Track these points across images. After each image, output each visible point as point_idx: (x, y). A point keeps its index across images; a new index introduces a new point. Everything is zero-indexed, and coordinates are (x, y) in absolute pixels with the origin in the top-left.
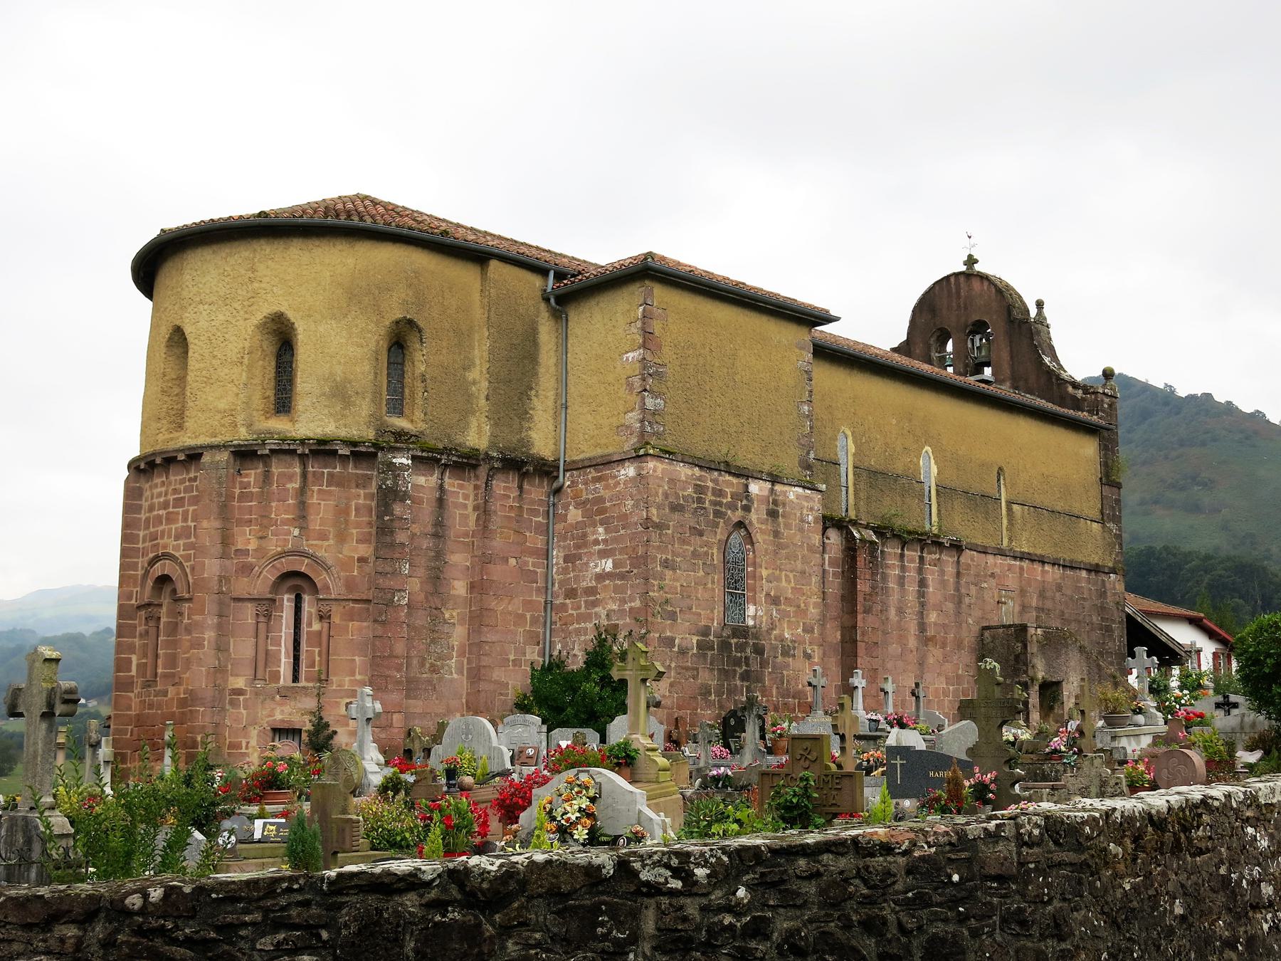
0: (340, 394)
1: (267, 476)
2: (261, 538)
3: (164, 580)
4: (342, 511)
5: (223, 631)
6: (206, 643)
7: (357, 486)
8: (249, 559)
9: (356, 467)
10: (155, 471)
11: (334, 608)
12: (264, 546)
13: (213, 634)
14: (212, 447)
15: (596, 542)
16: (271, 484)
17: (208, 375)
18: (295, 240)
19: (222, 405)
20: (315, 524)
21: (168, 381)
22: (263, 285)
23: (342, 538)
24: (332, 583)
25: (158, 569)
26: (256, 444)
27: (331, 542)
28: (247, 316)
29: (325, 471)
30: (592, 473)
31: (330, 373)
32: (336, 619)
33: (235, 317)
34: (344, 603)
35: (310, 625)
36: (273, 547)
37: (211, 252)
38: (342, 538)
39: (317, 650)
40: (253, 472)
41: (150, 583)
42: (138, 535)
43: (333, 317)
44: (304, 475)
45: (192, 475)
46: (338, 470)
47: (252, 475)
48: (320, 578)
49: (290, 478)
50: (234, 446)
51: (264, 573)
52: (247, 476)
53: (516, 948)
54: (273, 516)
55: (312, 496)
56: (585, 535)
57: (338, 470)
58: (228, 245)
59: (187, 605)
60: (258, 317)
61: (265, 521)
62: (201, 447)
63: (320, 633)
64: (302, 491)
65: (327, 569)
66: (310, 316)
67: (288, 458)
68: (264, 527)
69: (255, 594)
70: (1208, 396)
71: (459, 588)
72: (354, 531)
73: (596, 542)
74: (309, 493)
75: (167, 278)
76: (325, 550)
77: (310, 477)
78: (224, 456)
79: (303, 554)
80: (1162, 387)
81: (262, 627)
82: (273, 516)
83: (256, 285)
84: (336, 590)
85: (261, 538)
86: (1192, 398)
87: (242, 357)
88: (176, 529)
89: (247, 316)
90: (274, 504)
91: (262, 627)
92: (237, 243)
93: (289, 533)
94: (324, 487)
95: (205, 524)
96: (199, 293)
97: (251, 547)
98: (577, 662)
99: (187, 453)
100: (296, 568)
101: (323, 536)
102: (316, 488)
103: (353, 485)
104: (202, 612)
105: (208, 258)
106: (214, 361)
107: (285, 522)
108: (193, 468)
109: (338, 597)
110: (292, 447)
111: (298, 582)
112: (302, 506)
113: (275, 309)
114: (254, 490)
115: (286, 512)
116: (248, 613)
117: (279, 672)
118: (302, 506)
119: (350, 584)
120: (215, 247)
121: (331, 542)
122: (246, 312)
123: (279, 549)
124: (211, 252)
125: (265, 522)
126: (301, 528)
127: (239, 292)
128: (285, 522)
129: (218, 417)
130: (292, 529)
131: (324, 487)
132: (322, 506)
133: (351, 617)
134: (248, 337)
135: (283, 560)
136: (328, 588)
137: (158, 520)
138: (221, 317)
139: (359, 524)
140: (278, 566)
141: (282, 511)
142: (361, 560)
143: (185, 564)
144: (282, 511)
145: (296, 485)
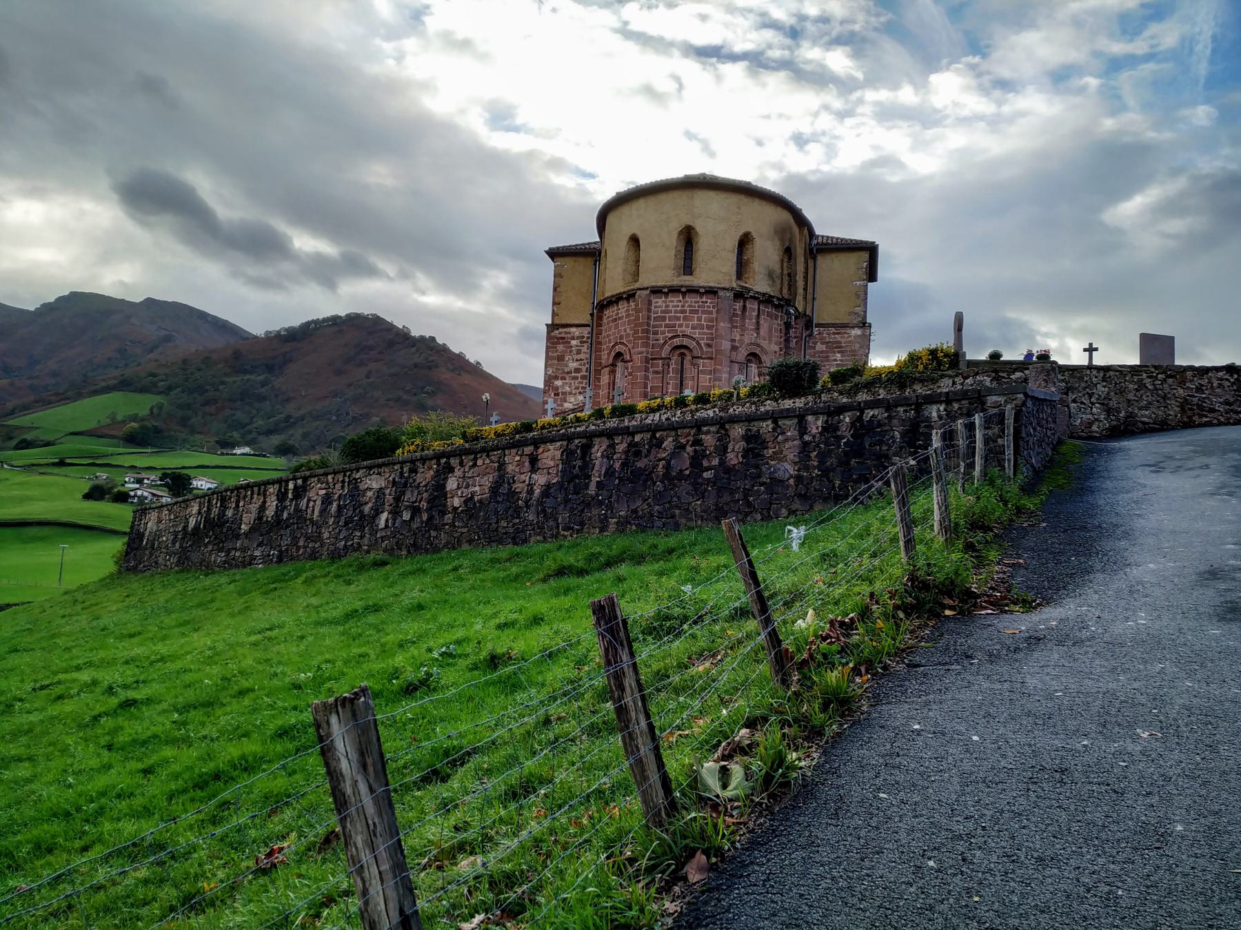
3: (619, 355)
14: (724, 289)
15: (836, 360)
20: (762, 332)
23: (770, 341)
25: (618, 349)
30: (833, 330)
41: (613, 354)
45: (704, 300)
48: (764, 358)
49: (754, 310)
53: (834, 679)
56: (828, 357)
65: (766, 353)
68: (743, 330)
70: (433, 339)
71: (514, 570)
73: (836, 360)
76: (764, 344)
78: (730, 294)
79: (758, 345)
80: (472, 361)
86: (422, 338)
95: (722, 324)
139: (777, 336)
141: (750, 324)
144: (750, 324)
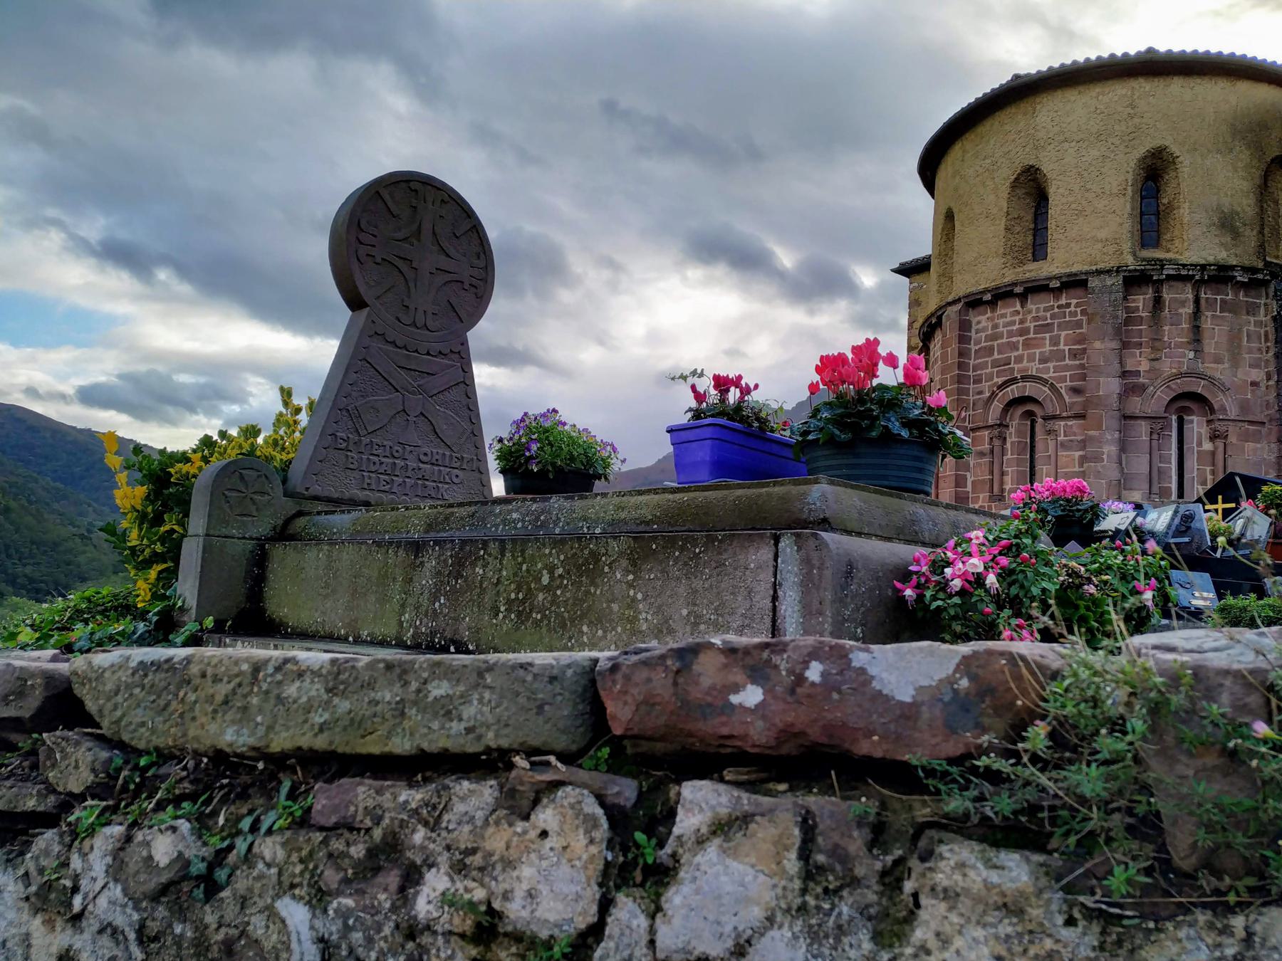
0: (1227, 224)
1: (1158, 302)
2: (1153, 360)
4: (1234, 339)
5: (1123, 447)
6: (1105, 457)
7: (1248, 313)
8: (1141, 380)
9: (1246, 296)
10: (999, 303)
11: (1230, 429)
12: (1157, 367)
13: (1113, 448)
14: (1099, 272)
16: (1162, 310)
17: (1079, 208)
18: (1176, 79)
19: (1102, 234)
20: (1209, 346)
21: (1011, 220)
22: (1144, 120)
24: (1228, 404)
26: (1153, 270)
27: (1226, 365)
28: (1128, 150)
29: (1218, 297)
31: (1218, 205)
32: (1233, 439)
33: (1113, 151)
34: (1241, 424)
35: (1200, 444)
36: (1167, 367)
37: (1077, 93)
38: (1235, 362)
39: (1208, 469)
40: (1141, 297)
42: (970, 349)
43: (1219, 151)
44: (1197, 301)
46: (1230, 297)
47: (1141, 301)
48: (1217, 399)
49: (1183, 303)
50: (1130, 271)
51: (1158, 393)
52: (1134, 301)
54: (1166, 339)
55: (1206, 321)
57: (1230, 297)
58: (1100, 85)
59: (1062, 423)
60: (1141, 151)
61: (1157, 344)
62: (1087, 273)
63: (1213, 453)
64: (1197, 314)
66: (1196, 150)
67: (1180, 285)
69: (1150, 411)
72: (1247, 356)
74: (1203, 318)
75: (944, 176)
76: (1220, 371)
77: (1203, 302)
79: (1201, 376)
81: (1155, 443)
82: (1166, 339)
83: (1136, 120)
84: (1233, 412)
85: (1153, 360)
87: (1125, 189)
88: (1040, 353)
89: (1128, 150)
90: (1166, 328)
91: (1155, 443)
92: (1115, 81)
93: (1184, 356)
94: (1218, 313)
96: (1063, 132)
97: (1141, 369)
98: (694, 404)
99: (1064, 279)
100: (1193, 389)
101: (1218, 360)
102: (1209, 314)
103: (1244, 312)
104: (1100, 428)
105: (1073, 98)
106: (1087, 195)
107: (1179, 345)
108: (1064, 295)
109: (1237, 418)
110: (1191, 273)
111: (1030, 407)
112: (1196, 329)
113: (1157, 143)
114: (1143, 315)
115: (1179, 336)
116: (1143, 428)
117: (1170, 488)
118: (1196, 329)
119: (1244, 407)
120: (1081, 88)
121: (1226, 365)
122: (1127, 146)
123: (1174, 371)
124: (1077, 93)
125: (1156, 344)
126: (1196, 351)
127: (1117, 127)
128: (1179, 345)
129: (1099, 246)
130: (1187, 352)
131: (1218, 313)
132: (1216, 330)
133: (1246, 437)
134: (1130, 170)
135: (1179, 381)
136: (1225, 409)
137: (1014, 347)
138: (1095, 153)
140: (1174, 386)
141: (1175, 333)
142: (1254, 384)
143: (1058, 386)
144: (1175, 333)
145: (1188, 310)
